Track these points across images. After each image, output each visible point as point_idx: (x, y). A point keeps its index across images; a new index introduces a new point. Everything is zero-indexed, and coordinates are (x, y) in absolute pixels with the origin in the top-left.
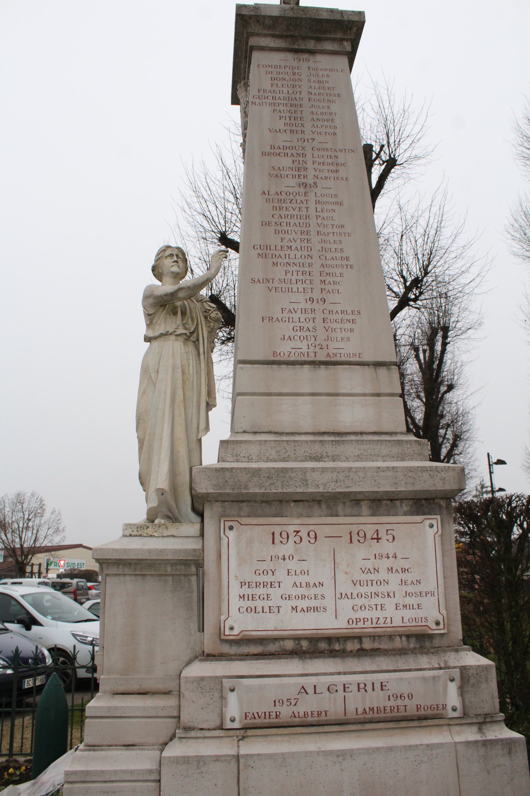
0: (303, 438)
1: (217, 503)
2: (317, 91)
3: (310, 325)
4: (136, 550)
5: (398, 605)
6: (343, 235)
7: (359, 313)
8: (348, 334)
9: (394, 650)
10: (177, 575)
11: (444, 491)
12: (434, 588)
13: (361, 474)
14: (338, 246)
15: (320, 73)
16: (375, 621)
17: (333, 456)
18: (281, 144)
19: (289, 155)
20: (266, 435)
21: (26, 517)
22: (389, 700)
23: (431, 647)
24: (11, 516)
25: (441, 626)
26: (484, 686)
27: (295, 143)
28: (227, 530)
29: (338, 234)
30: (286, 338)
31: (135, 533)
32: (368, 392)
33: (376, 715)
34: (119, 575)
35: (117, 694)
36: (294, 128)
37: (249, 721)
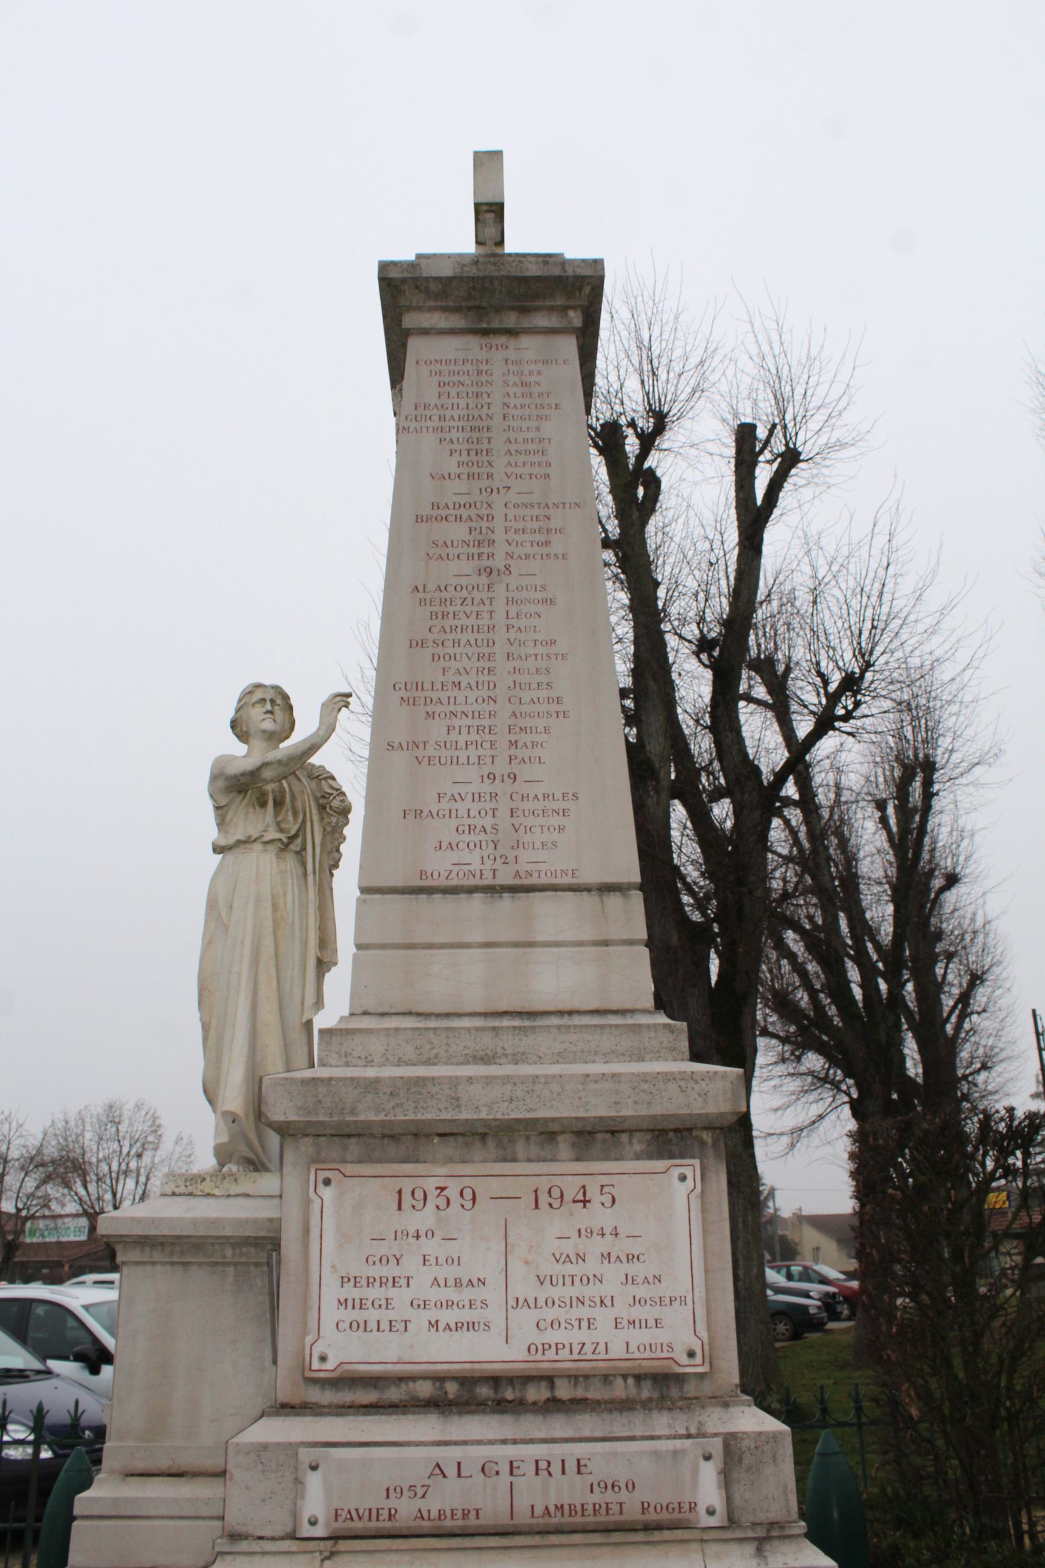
0: (466, 1023)
1: (306, 1139)
2: (518, 402)
3: (488, 822)
4: (171, 1220)
5: (619, 1320)
6: (553, 657)
7: (575, 796)
8: (555, 836)
9: (612, 1401)
10: (243, 1264)
11: (707, 1114)
12: (687, 1291)
13: (555, 1087)
14: (543, 678)
15: (526, 368)
16: (576, 1348)
17: (514, 1055)
18: (451, 500)
19: (464, 519)
20: (401, 1018)
21: (125, 1150)
22: (592, 1491)
23: (681, 1397)
24: (95, 1148)
25: (698, 1359)
28: (320, 1185)
29: (545, 657)
30: (444, 846)
31: (182, 1189)
32: (585, 939)
33: (567, 1519)
34: (144, 1263)
35: (132, 1475)
36: (475, 470)
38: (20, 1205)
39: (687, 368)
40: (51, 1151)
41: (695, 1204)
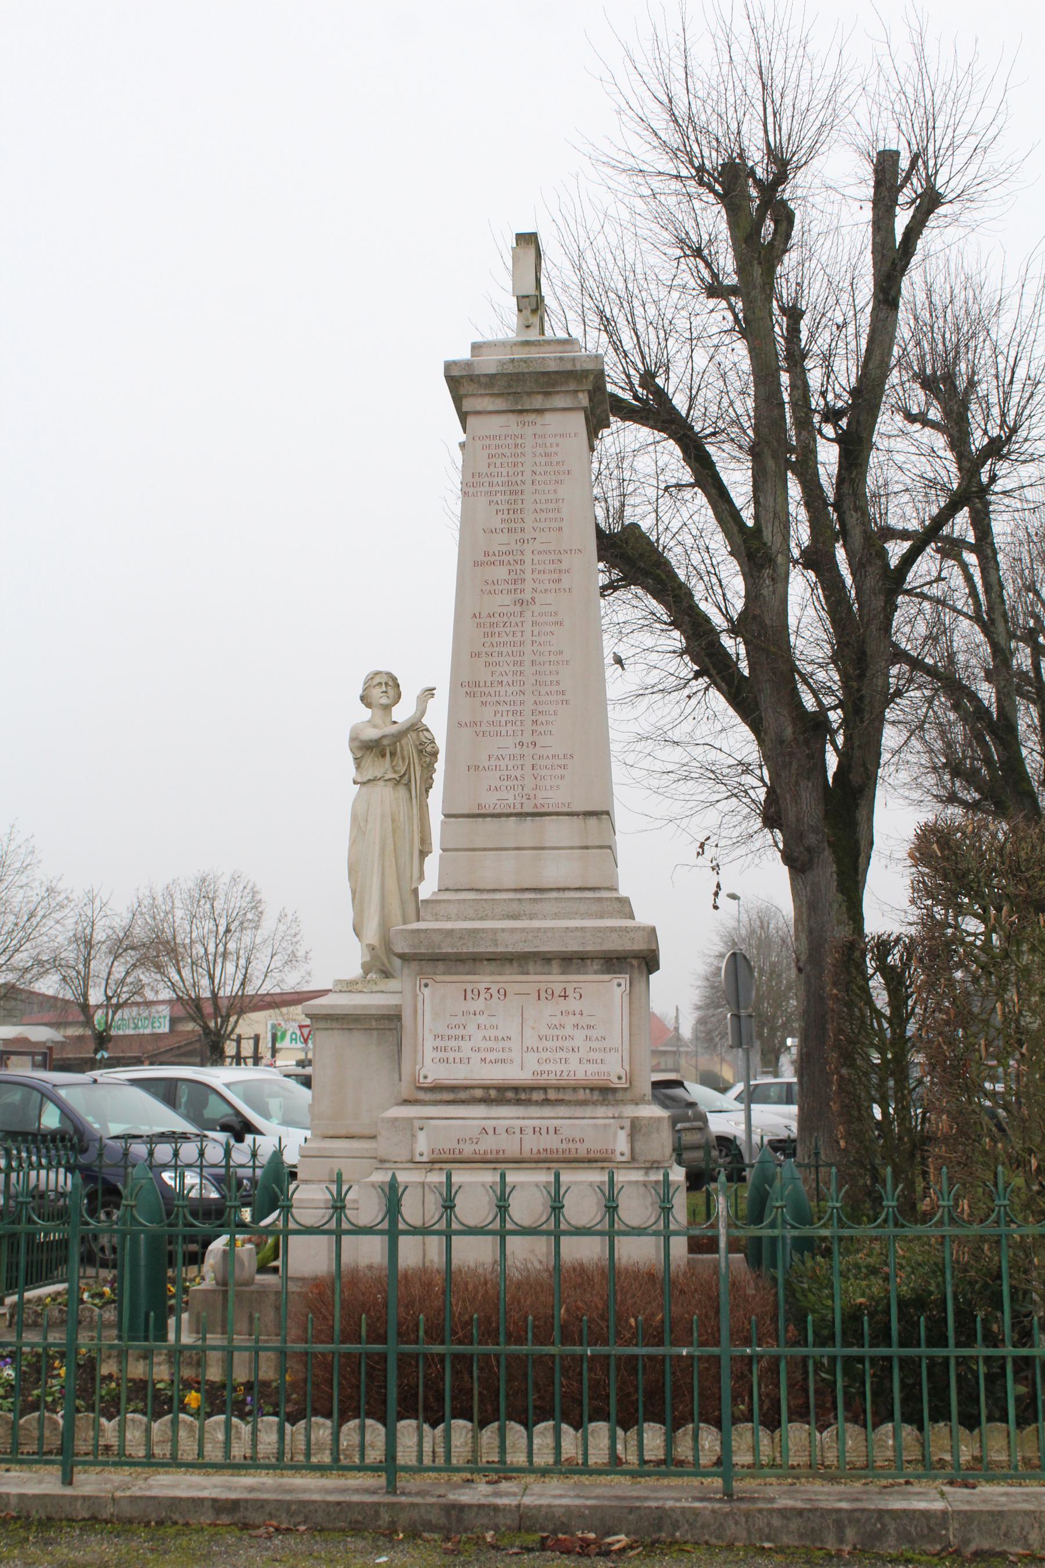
2: (542, 469)
3: (518, 773)
8: (558, 782)
14: (554, 678)
18: (496, 548)
26: (655, 1135)
27: (514, 546)
36: (513, 525)
37: (435, 1156)
38: (110, 994)
39: (814, 103)
40: (140, 933)
41: (626, 998)
